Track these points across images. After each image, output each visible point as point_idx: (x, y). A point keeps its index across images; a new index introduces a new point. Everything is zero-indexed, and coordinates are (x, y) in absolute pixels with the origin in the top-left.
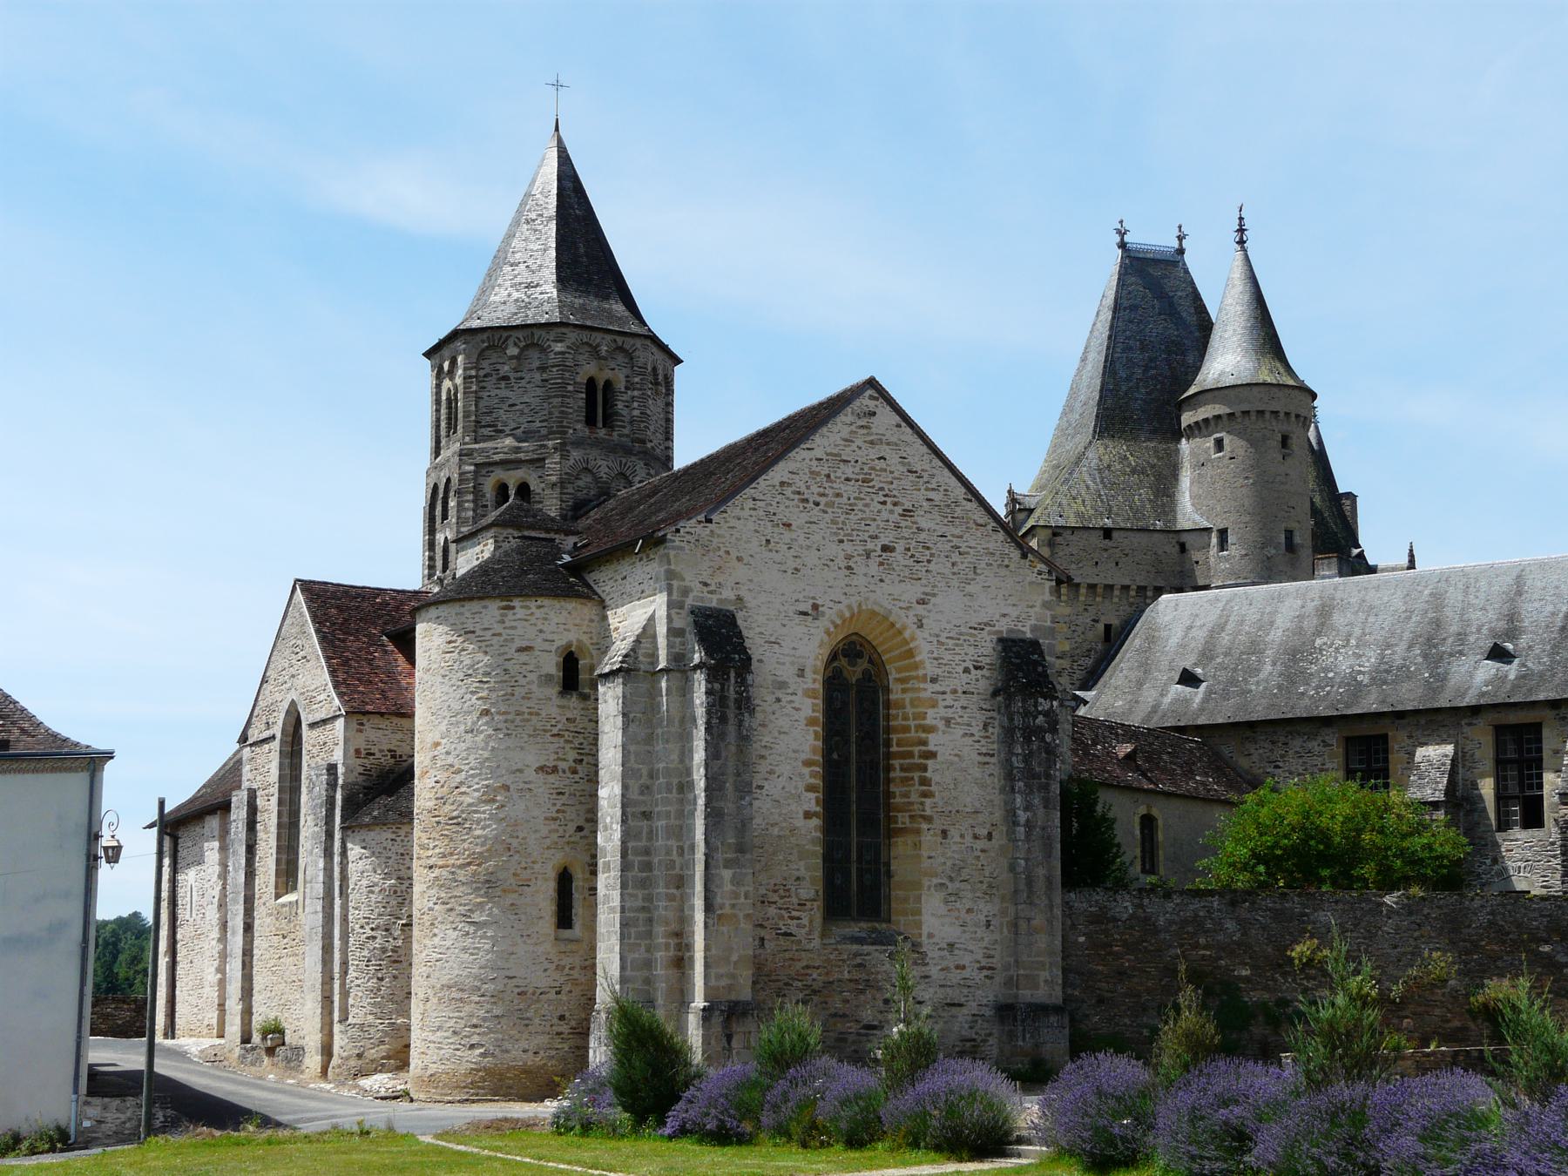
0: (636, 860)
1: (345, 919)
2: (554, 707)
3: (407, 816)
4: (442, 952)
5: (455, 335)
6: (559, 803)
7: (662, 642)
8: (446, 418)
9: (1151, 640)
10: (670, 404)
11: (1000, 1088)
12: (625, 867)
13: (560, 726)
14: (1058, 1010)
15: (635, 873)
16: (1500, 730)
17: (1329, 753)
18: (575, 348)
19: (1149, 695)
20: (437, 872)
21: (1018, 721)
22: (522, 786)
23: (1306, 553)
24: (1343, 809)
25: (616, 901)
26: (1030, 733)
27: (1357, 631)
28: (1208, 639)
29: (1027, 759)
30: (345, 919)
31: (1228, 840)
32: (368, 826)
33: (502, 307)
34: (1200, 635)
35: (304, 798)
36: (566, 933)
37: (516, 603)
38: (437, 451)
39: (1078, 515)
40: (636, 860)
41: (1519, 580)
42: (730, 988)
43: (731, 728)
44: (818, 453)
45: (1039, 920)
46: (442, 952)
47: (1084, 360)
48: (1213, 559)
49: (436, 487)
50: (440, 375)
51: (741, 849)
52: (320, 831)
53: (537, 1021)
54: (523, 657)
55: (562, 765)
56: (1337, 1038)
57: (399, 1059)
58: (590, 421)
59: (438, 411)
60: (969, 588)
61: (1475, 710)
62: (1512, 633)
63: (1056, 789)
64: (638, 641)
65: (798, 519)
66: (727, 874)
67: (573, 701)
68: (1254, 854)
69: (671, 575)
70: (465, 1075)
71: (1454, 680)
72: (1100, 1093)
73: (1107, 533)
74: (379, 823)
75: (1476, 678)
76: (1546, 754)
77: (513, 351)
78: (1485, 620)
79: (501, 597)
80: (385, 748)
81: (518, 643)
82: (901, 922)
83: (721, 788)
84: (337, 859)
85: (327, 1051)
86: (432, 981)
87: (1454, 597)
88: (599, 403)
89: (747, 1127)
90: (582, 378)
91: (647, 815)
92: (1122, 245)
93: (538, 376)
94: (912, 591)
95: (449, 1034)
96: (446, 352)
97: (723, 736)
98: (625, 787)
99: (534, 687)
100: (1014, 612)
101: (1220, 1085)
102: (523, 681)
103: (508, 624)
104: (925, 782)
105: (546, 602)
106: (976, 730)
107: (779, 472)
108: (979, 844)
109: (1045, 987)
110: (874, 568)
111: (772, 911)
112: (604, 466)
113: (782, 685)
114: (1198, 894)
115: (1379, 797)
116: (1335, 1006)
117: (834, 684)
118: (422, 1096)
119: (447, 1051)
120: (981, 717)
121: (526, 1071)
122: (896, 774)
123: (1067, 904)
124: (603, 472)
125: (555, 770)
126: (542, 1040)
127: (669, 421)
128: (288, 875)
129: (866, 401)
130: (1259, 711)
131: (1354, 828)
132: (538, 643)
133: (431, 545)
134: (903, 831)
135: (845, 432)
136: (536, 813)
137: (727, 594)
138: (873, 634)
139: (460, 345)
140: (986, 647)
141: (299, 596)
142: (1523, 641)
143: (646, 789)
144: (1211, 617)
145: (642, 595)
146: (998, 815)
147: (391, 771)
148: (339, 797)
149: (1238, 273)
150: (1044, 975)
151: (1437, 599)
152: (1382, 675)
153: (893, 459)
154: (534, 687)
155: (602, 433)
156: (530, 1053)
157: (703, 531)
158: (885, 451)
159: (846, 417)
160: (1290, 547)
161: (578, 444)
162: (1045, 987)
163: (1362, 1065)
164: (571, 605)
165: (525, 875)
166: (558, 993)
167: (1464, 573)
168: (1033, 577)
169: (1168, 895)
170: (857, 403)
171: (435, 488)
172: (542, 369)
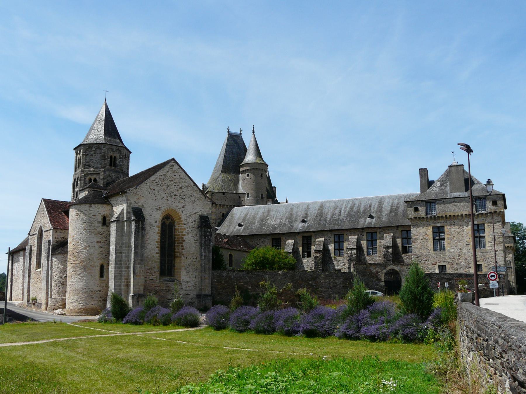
2: (100, 228)
3: (66, 252)
4: (74, 282)
5: (81, 145)
7: (125, 215)
8: (78, 163)
9: (232, 217)
10: (129, 162)
11: (194, 311)
12: (116, 264)
14: (210, 296)
18: (108, 149)
19: (231, 229)
21: (203, 234)
23: (265, 199)
25: (113, 272)
26: (206, 236)
28: (244, 217)
29: (205, 242)
31: (248, 260)
34: (243, 216)
36: (102, 279)
37: (93, 205)
38: (76, 171)
41: (308, 206)
42: (139, 291)
43: (140, 234)
45: (207, 277)
46: (74, 282)
48: (246, 200)
50: (77, 154)
52: (46, 255)
54: (94, 217)
55: (102, 241)
57: (63, 306)
58: (111, 165)
61: (299, 233)
62: (306, 217)
63: (211, 248)
64: (120, 214)
66: (138, 266)
67: (105, 227)
69: (128, 200)
72: (218, 313)
73: (224, 193)
75: (299, 226)
76: (312, 242)
77: (94, 149)
78: (301, 214)
79: (89, 203)
81: (93, 214)
82: (177, 277)
83: (138, 247)
85: (47, 304)
87: (295, 209)
88: (113, 161)
89: (142, 321)
90: (109, 156)
92: (228, 132)
93: (99, 155)
94: (181, 205)
96: (78, 149)
97: (138, 235)
100: (203, 210)
101: (243, 312)
104: (182, 246)
106: (194, 235)
108: (194, 260)
109: (208, 291)
110: (173, 200)
111: (148, 274)
113: (152, 225)
114: (240, 271)
115: (279, 251)
119: (74, 305)
120: (196, 232)
121: (92, 309)
122: (176, 245)
123: (213, 273)
125: (100, 242)
126: (96, 302)
127: (128, 166)
128: (39, 265)
129: (172, 163)
131: (273, 257)
132: (97, 214)
133: (74, 192)
134: (178, 257)
135: (167, 170)
137: (140, 204)
139: (82, 147)
140: (197, 217)
141: (43, 202)
142: (309, 219)
144: (245, 212)
146: (198, 254)
148: (51, 247)
149: (253, 139)
150: (207, 288)
152: (280, 225)
153: (178, 176)
155: (113, 168)
157: (135, 190)
158: (176, 174)
159: (167, 166)
161: (108, 170)
162: (208, 291)
164: (105, 206)
167: (297, 204)
168: (207, 202)
171: (75, 179)
172: (100, 153)
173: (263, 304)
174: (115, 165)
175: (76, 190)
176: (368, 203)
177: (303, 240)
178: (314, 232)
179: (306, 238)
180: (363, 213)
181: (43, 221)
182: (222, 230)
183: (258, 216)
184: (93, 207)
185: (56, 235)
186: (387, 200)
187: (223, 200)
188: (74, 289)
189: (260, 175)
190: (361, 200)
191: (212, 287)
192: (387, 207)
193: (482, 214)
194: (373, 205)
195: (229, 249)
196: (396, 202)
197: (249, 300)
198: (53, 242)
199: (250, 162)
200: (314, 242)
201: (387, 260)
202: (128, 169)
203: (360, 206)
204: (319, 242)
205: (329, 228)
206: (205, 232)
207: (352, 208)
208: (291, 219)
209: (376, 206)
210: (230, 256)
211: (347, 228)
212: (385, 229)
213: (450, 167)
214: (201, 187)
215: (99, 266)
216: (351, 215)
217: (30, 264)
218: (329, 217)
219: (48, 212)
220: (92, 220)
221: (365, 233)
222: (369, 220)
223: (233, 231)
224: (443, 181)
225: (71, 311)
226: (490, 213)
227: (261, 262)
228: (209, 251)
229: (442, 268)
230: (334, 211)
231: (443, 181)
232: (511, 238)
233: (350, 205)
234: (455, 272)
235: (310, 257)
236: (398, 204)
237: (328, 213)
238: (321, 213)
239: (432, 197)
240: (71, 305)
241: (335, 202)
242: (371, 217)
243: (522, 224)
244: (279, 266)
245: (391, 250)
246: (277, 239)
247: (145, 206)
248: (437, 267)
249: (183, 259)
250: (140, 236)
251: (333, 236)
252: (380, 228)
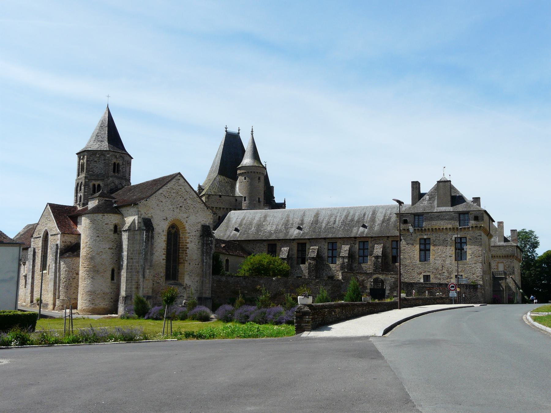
0: (130, 268)
2: (112, 236)
3: (78, 255)
4: (84, 285)
5: (85, 151)
7: (136, 224)
8: (81, 168)
9: (229, 221)
10: (130, 168)
11: (208, 310)
12: (127, 269)
14: (210, 298)
15: (129, 270)
16: (298, 244)
17: (265, 247)
18: (112, 156)
19: (228, 233)
21: (205, 242)
23: (262, 203)
24: (267, 260)
25: (125, 276)
26: (207, 244)
27: (272, 222)
28: (241, 221)
29: (206, 249)
31: (245, 265)
32: (66, 258)
33: (95, 147)
34: (239, 220)
35: (49, 251)
36: (113, 282)
37: (105, 214)
38: (78, 175)
39: (214, 192)
40: (130, 268)
41: (304, 215)
42: (148, 293)
43: (150, 242)
44: (168, 187)
45: (207, 281)
46: (84, 285)
47: (216, 156)
48: (244, 204)
50: (80, 159)
51: (151, 266)
52: (54, 258)
54: (106, 226)
56: (263, 302)
57: (76, 308)
58: (114, 172)
60: (197, 215)
61: (294, 240)
62: (302, 224)
63: (212, 255)
64: (131, 224)
65: (164, 201)
66: (148, 271)
67: (116, 235)
68: (249, 269)
69: (139, 211)
71: (290, 233)
72: (226, 311)
73: (220, 196)
74: (69, 257)
75: (294, 233)
76: (307, 249)
77: (98, 156)
78: (297, 220)
79: (102, 213)
82: (180, 281)
83: (147, 254)
85: (54, 305)
87: (291, 216)
88: (116, 168)
89: (161, 317)
90: (113, 162)
91: (132, 259)
92: (226, 131)
93: (103, 161)
94: (185, 215)
96: (82, 154)
97: (148, 244)
98: (128, 253)
100: (205, 220)
101: (245, 309)
104: (186, 253)
105: (111, 214)
106: (197, 243)
107: (160, 191)
108: (196, 266)
109: (208, 294)
110: (178, 211)
111: (156, 278)
112: (117, 182)
113: (159, 234)
114: (238, 276)
115: (274, 258)
116: (262, 297)
117: (169, 233)
120: (198, 241)
121: (104, 309)
122: (181, 251)
123: (213, 278)
124: (117, 183)
125: (112, 249)
126: (107, 303)
127: (130, 171)
128: (44, 266)
129: (178, 177)
130: (251, 238)
131: (269, 263)
132: (110, 223)
133: (76, 196)
134: (182, 263)
135: (174, 183)
137: (150, 215)
138: (177, 224)
139: (85, 153)
140: (199, 227)
141: (48, 207)
142: (304, 226)
143: (132, 254)
144: (241, 217)
145: (132, 215)
146: (200, 260)
149: (251, 141)
150: (208, 292)
151: (288, 216)
152: (276, 231)
153: (183, 189)
155: (116, 174)
157: (145, 202)
158: (181, 187)
159: (174, 180)
160: (259, 201)
161: (111, 177)
162: (208, 294)
163: (266, 306)
164: (116, 215)
167: (294, 210)
168: (209, 213)
169: (232, 277)
170: (176, 178)
171: (78, 184)
172: (104, 160)
173: (260, 303)
174: (118, 171)
175: (79, 195)
176: (363, 213)
177: (298, 247)
178: (309, 239)
179: (301, 245)
180: (357, 222)
181: (48, 225)
182: (218, 233)
183: (255, 221)
184: (106, 217)
186: (381, 210)
187: (219, 200)
189: (257, 179)
190: (355, 209)
191: (212, 291)
192: (380, 217)
193: (465, 228)
194: (367, 214)
195: (226, 254)
196: (389, 212)
197: (251, 302)
199: (248, 165)
200: (309, 249)
201: (376, 269)
202: (130, 175)
203: (354, 215)
204: (313, 249)
205: (323, 236)
206: (207, 241)
207: (347, 216)
208: (287, 225)
209: (370, 216)
210: (227, 260)
211: (340, 236)
212: (376, 239)
213: (438, 182)
214: (196, 189)
215: (110, 269)
216: (346, 224)
217: (34, 266)
218: (324, 225)
219: (54, 217)
221: (357, 242)
222: (362, 229)
223: (229, 236)
224: (431, 195)
225: (81, 310)
226: (472, 227)
227: (257, 268)
228: (210, 258)
229: (427, 278)
230: (329, 219)
231: (431, 195)
232: (513, 248)
233: (345, 214)
234: (437, 281)
235: (305, 264)
236: (391, 214)
237: (323, 220)
238: (316, 221)
239: (420, 211)
240: (84, 305)
241: (331, 210)
242: (364, 226)
243: (533, 232)
244: (274, 272)
245: (380, 260)
246: (272, 246)
247: (154, 217)
248: (422, 276)
249: (186, 265)
250: (150, 242)
251: (327, 244)
252: (372, 237)
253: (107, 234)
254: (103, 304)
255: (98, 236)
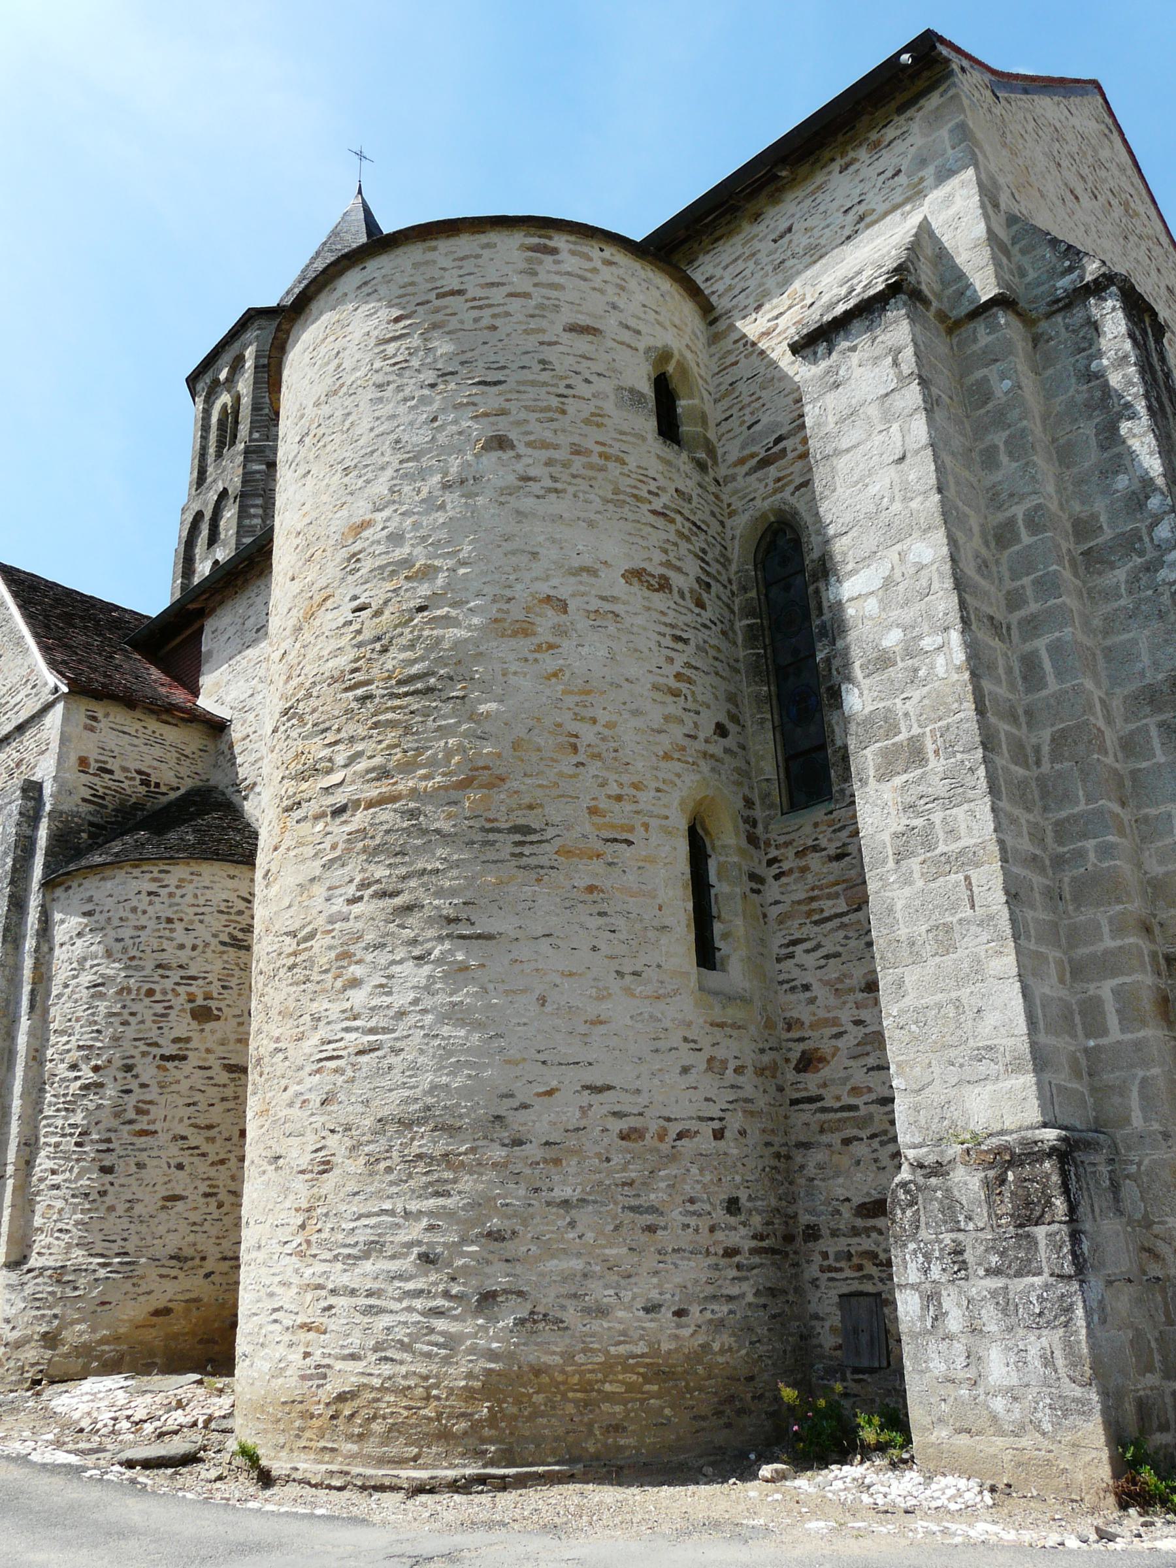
1: (37, 1057)
6: (680, 660)
13: (665, 498)
20: (360, 819)
22: (595, 604)
30: (37, 1057)
36: (713, 978)
49: (199, 516)
53: (676, 1216)
54: (582, 344)
55: (677, 580)
57: (208, 1348)
59: (204, 438)
70: (470, 1395)
80: (133, 765)
81: (567, 316)
84: (29, 944)
86: (342, 1112)
95: (407, 1264)
99: (609, 406)
102: (582, 389)
103: (543, 277)
118: (307, 1466)
119: (398, 1320)
121: (660, 1372)
125: (664, 585)
132: (610, 324)
136: (634, 670)
147: (137, 806)
148: (43, 834)
154: (609, 406)
156: (666, 1314)
165: (620, 813)
166: (719, 1135)
184: (571, 263)
185: (89, 746)
188: (390, 1104)
198: (63, 789)
219: (29, 617)
220: (562, 363)
240: (346, 1328)
253: (596, 420)
254: (653, 1299)
255: (500, 443)
